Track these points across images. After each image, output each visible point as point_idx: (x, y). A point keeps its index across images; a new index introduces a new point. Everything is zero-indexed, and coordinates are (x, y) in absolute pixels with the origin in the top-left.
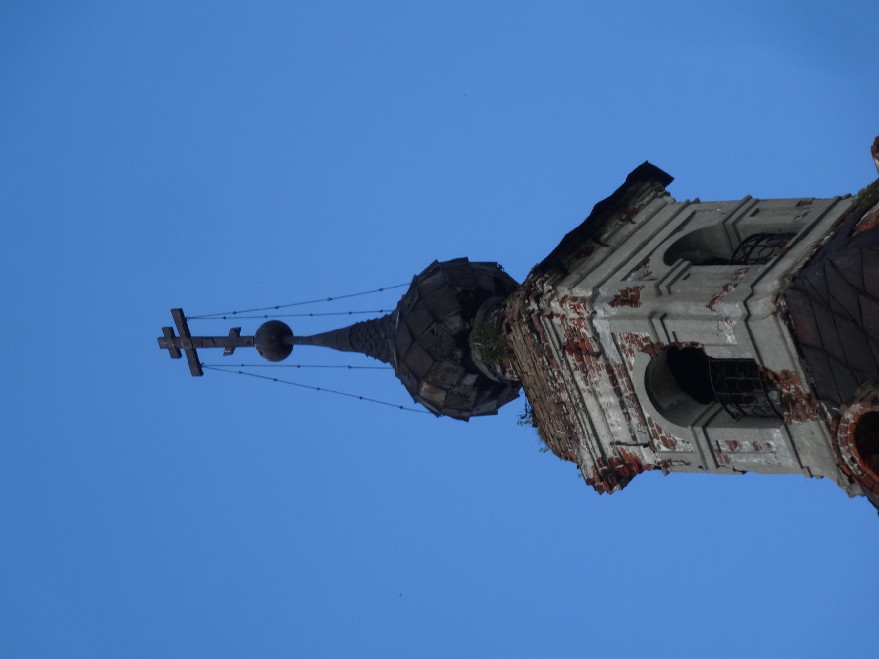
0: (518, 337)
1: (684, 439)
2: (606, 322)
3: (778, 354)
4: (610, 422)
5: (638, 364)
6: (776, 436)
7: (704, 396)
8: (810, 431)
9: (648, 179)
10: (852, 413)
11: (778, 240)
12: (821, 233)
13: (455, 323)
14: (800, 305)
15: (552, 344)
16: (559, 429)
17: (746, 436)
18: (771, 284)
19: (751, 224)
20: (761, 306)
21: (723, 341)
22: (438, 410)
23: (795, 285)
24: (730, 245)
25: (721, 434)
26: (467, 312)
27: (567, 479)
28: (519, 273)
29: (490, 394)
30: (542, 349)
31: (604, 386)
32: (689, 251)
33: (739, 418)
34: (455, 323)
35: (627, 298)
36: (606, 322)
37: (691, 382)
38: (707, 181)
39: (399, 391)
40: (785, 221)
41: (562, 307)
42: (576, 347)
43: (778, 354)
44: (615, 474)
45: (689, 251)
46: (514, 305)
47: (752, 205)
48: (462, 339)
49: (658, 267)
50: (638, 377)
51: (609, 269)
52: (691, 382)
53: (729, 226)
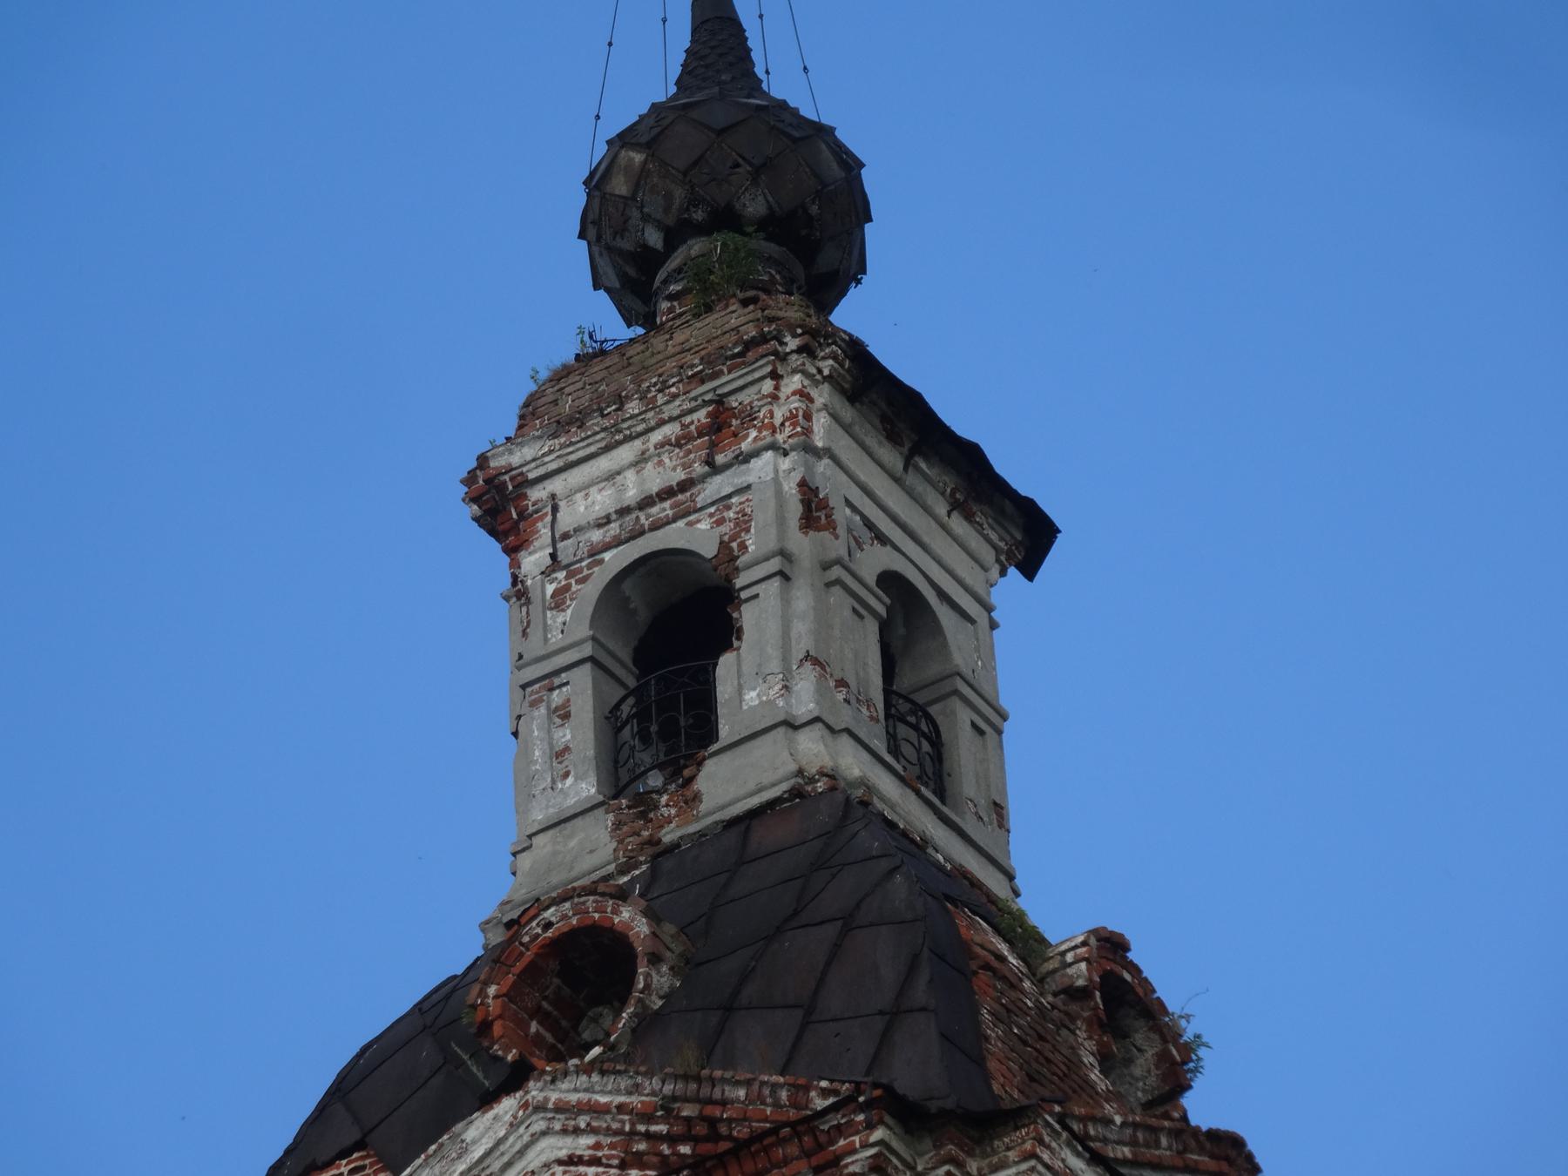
0: (735, 319)
1: (569, 626)
2: (769, 473)
3: (728, 783)
4: (595, 493)
5: (699, 536)
6: (584, 788)
7: (646, 656)
8: (594, 847)
9: (1029, 536)
10: (631, 919)
11: (931, 773)
12: (949, 848)
13: (754, 206)
14: (818, 820)
15: (727, 381)
16: (575, 401)
17: (581, 735)
18: (853, 764)
19: (958, 722)
20: (813, 749)
21: (747, 685)
22: (596, 183)
23: (852, 807)
24: (919, 690)
25: (581, 691)
26: (776, 225)
27: (486, 422)
28: (849, 315)
29: (631, 276)
30: (715, 362)
31: (656, 478)
32: (905, 615)
33: (611, 721)
34: (754, 206)
35: (814, 511)
36: (769, 473)
37: (671, 632)
38: (1030, 642)
39: (626, 112)
40: (967, 783)
41: (792, 394)
42: (723, 421)
43: (728, 783)
44: (500, 506)
45: (905, 615)
46: (791, 309)
47: (991, 722)
48: (725, 219)
49: (873, 561)
50: (674, 537)
51: (863, 473)
52: (671, 632)
53: (951, 684)
